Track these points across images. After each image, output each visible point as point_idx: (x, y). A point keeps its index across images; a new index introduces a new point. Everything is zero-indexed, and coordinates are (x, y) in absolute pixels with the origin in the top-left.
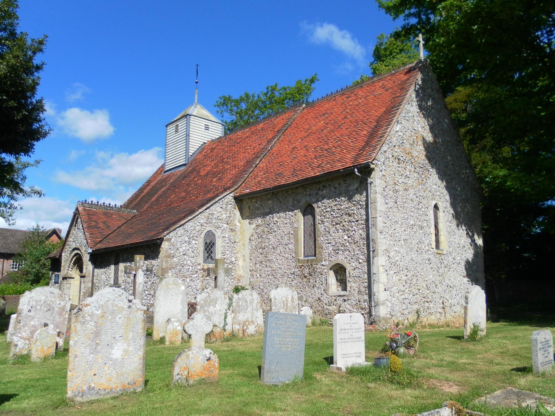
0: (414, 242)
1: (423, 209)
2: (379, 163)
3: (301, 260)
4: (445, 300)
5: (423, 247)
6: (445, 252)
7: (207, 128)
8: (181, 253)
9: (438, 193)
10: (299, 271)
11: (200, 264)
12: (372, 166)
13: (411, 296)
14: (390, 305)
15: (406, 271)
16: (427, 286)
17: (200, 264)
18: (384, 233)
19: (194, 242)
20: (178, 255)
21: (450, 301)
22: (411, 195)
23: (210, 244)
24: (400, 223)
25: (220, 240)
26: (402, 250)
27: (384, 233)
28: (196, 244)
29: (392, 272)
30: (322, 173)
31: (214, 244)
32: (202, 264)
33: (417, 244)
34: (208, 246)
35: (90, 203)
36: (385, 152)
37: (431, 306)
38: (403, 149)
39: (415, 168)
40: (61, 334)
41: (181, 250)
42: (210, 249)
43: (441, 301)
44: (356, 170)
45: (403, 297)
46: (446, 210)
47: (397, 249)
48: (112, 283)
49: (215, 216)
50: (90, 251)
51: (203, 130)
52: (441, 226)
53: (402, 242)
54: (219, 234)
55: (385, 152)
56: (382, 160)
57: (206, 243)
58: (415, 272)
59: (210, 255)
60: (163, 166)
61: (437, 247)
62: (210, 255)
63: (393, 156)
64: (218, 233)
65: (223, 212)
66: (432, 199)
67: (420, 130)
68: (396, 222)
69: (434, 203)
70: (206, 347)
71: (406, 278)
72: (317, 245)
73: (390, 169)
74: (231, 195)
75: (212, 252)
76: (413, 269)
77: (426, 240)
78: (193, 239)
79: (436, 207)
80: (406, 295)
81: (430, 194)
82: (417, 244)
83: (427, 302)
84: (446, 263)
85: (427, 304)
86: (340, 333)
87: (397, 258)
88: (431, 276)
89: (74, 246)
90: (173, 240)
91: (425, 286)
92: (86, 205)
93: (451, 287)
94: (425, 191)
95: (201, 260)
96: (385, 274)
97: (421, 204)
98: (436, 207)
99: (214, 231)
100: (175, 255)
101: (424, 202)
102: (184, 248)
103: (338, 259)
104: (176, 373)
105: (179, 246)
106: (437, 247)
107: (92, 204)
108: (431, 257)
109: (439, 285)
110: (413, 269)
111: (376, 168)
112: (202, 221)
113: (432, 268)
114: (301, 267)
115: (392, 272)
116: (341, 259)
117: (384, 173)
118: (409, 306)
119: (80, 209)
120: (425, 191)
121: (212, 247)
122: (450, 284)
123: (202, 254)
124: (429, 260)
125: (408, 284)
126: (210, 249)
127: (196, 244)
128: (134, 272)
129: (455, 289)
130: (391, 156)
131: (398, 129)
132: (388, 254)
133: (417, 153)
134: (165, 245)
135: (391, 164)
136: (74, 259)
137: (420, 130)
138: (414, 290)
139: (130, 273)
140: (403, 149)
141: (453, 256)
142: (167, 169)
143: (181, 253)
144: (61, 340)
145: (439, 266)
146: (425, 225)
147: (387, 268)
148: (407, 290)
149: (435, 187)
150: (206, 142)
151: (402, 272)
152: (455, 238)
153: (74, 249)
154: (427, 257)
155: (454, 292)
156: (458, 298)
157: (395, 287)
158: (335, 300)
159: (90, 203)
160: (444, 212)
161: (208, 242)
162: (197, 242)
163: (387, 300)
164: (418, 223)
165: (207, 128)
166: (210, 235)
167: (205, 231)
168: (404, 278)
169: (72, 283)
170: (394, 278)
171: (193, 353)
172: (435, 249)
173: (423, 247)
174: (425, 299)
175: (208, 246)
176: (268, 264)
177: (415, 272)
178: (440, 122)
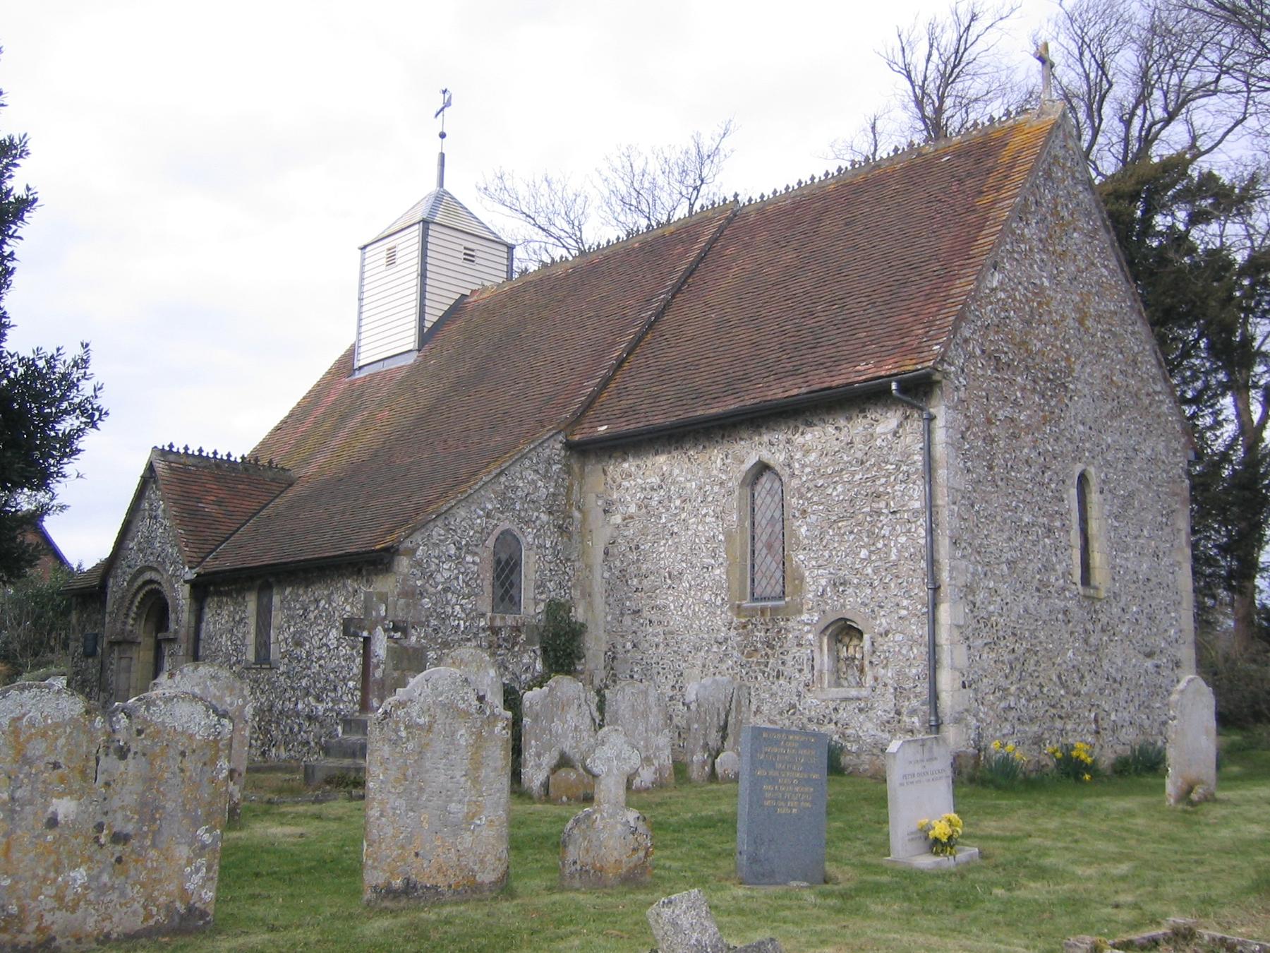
0: (1030, 567)
1: (1053, 486)
2: (953, 369)
3: (746, 609)
4: (1102, 714)
5: (1053, 579)
6: (1103, 594)
7: (469, 257)
8: (440, 587)
9: (1087, 445)
10: (739, 635)
11: (483, 615)
12: (937, 377)
13: (1023, 701)
14: (973, 722)
15: (1012, 639)
16: (1059, 677)
17: (483, 615)
18: (963, 545)
19: (469, 558)
20: (432, 590)
21: (1113, 717)
22: (1026, 450)
23: (507, 563)
24: (999, 518)
25: (531, 553)
26: (1003, 588)
27: (963, 545)
28: (474, 563)
29: (979, 642)
30: (804, 390)
31: (518, 564)
32: (489, 614)
33: (1039, 571)
34: (503, 570)
35: (182, 451)
36: (966, 341)
37: (1069, 727)
38: (1007, 334)
39: (1034, 381)
40: (236, 775)
41: (439, 578)
42: (507, 577)
43: (1093, 715)
44: (894, 386)
45: (1003, 705)
46: (1106, 488)
47: (992, 584)
48: (251, 657)
49: (519, 493)
50: (190, 575)
51: (460, 262)
52: (1094, 526)
53: (1004, 567)
54: (530, 539)
55: (966, 341)
56: (960, 362)
57: (498, 562)
58: (1034, 642)
59: (507, 592)
60: (351, 353)
61: (1086, 579)
62: (507, 592)
63: (983, 352)
64: (528, 537)
65: (540, 483)
66: (1074, 459)
67: (1046, 283)
68: (991, 518)
69: (1078, 468)
70: (628, 805)
71: (1012, 657)
72: (788, 571)
73: (977, 384)
74: (561, 438)
75: (512, 585)
76: (1027, 634)
77: (1060, 562)
78: (468, 552)
79: (1083, 479)
80: (1012, 698)
81: (1070, 447)
82: (1039, 571)
83: (1060, 717)
84: (1104, 620)
85: (1058, 724)
86: (902, 784)
87: (991, 608)
88: (1070, 653)
89: (140, 564)
90: (419, 552)
91: (1054, 678)
92: (171, 458)
93: (1115, 681)
94: (1057, 440)
95: (485, 605)
96: (964, 647)
97: (1048, 473)
98: (1083, 479)
99: (517, 532)
100: (426, 591)
101: (1056, 465)
102: (446, 574)
103: (843, 606)
104: (571, 860)
105: (433, 567)
106: (1086, 579)
107: (186, 453)
108: (1070, 604)
109: (1088, 677)
110: (1027, 634)
111: (944, 381)
112: (490, 506)
113: (1072, 633)
114: (745, 627)
115: (979, 642)
116: (852, 605)
117: (962, 394)
118: (1018, 727)
119: (160, 466)
120: (1057, 440)
121: (512, 572)
122: (1114, 674)
123: (488, 589)
124: (1065, 612)
125: (1016, 674)
126: (507, 577)
127: (474, 563)
128: (365, 634)
129: (1125, 686)
130: (978, 352)
131: (995, 284)
132: (970, 598)
133: (1039, 345)
134: (403, 564)
135: (980, 372)
136: (141, 595)
137: (1046, 283)
138: (1029, 688)
139: (356, 635)
140: (1007, 334)
141: (1122, 604)
142: (361, 364)
143: (440, 587)
144: (237, 788)
145: (1090, 627)
146: (1058, 524)
147: (969, 632)
148: (1013, 689)
149: (1081, 428)
150: (468, 293)
151: (1002, 643)
152: (1127, 559)
153: (142, 571)
154: (1062, 604)
155: (1123, 694)
156: (1132, 709)
157: (985, 680)
158: (836, 710)
159: (182, 451)
160: (1101, 492)
161: (504, 557)
162: (477, 559)
163: (967, 710)
164: (1041, 520)
165: (469, 257)
166: (508, 541)
167: (497, 532)
168: (1007, 657)
169: (135, 656)
170: (985, 656)
171: (603, 818)
172: (1079, 586)
173: (1053, 579)
174: (1054, 711)
175: (503, 570)
176: (654, 618)
177: (1034, 642)
178: (1093, 264)
